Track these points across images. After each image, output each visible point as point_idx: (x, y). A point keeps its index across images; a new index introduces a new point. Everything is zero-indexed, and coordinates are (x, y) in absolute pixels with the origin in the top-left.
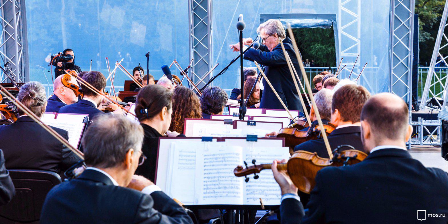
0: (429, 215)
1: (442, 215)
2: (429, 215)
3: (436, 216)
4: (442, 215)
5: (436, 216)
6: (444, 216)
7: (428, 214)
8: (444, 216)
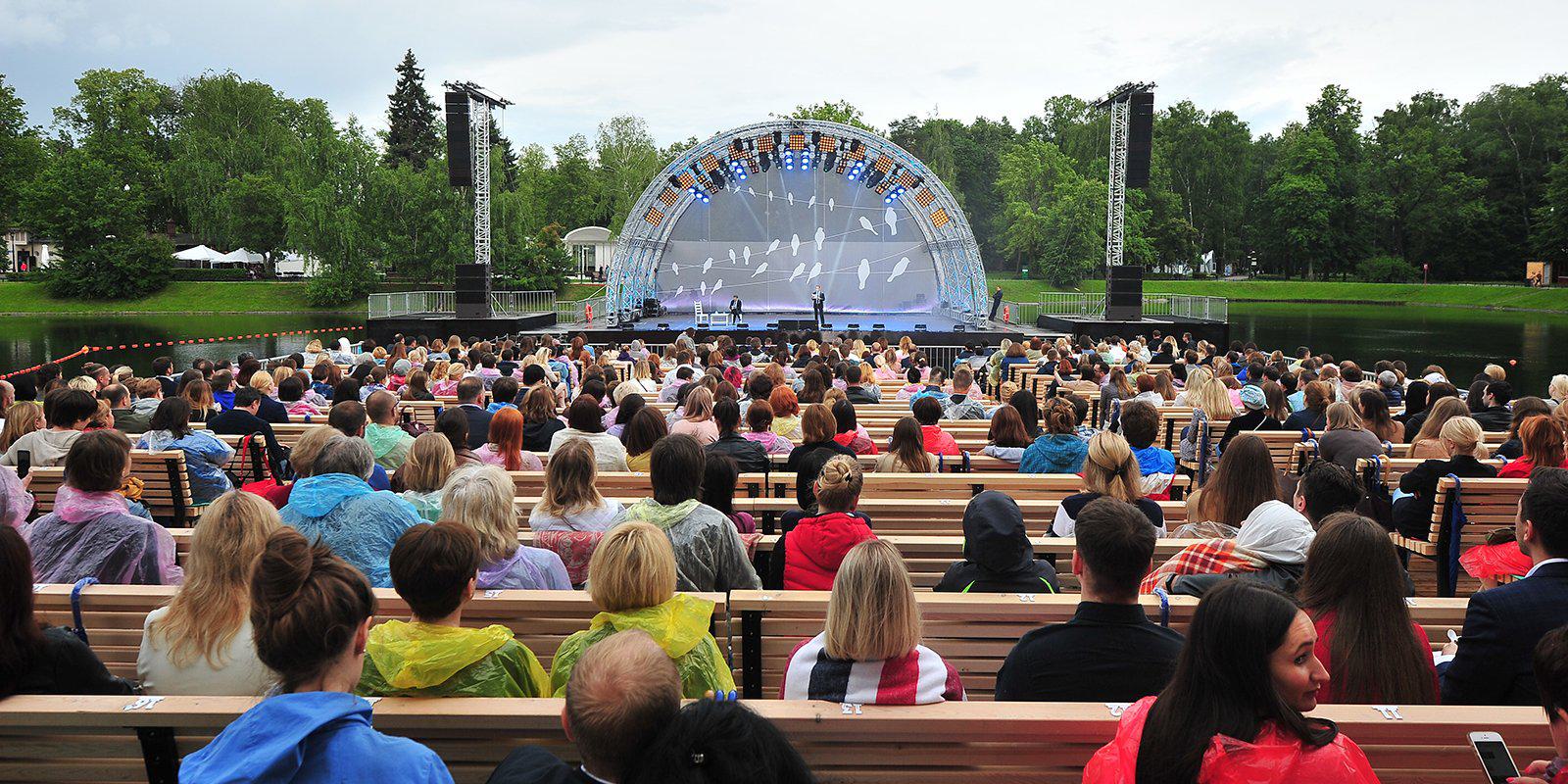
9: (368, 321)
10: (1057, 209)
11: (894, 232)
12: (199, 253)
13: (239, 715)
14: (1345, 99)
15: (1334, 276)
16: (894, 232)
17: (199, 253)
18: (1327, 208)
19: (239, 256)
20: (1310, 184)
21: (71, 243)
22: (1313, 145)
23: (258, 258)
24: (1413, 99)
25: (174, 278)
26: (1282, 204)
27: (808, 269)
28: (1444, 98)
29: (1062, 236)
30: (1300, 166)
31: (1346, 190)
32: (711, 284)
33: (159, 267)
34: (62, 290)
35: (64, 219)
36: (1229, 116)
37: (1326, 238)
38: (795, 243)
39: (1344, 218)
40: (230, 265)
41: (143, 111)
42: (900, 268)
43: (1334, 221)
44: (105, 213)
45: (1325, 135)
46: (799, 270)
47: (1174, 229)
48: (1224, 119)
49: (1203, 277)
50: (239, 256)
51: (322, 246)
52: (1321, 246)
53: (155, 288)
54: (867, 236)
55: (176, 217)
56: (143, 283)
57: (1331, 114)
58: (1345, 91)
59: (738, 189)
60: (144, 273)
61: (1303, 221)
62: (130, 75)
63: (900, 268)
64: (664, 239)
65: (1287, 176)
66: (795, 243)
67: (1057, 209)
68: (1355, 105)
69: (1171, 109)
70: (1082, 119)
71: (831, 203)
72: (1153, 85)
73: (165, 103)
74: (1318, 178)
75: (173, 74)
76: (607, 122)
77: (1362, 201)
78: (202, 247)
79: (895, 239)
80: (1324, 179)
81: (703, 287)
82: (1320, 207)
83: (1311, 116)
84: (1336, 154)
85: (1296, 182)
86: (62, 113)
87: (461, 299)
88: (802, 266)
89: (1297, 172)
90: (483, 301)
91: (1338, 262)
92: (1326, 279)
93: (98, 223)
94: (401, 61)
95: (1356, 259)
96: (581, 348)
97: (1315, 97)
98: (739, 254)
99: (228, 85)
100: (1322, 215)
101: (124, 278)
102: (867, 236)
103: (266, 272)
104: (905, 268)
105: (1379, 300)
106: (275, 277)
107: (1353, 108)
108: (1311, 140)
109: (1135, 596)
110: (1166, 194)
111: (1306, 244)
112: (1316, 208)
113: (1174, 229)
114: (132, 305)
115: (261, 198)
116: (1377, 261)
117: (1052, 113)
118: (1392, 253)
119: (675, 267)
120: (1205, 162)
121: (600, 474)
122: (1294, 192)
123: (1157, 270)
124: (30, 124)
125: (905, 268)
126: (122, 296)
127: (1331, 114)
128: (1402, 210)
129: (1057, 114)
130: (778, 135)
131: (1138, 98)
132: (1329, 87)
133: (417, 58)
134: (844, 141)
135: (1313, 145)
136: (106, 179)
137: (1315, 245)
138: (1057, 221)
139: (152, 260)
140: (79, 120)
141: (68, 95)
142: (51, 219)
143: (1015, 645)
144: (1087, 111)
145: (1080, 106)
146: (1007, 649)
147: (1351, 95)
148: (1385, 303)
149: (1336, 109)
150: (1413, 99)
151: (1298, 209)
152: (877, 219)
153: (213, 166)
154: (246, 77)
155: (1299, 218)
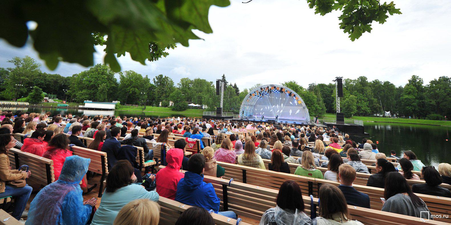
0: (432, 216)
1: (445, 216)
2: (432, 216)
3: (439, 217)
4: (445, 216)
5: (439, 217)
6: (447, 217)
7: (431, 215)
8: (447, 217)
9: (203, 116)
10: (345, 101)
11: (296, 105)
12: (192, 105)
13: (13, 147)
14: (418, 78)
15: (422, 118)
16: (296, 105)
17: (192, 105)
18: (416, 102)
19: (197, 105)
20: (410, 97)
21: (175, 102)
22: (410, 88)
23: (199, 106)
24: (439, 78)
25: (188, 108)
26: (404, 101)
27: (280, 111)
28: (448, 77)
29: (346, 107)
30: (407, 93)
31: (421, 98)
32: (262, 113)
33: (185, 107)
34: (173, 110)
35: (174, 99)
36: (388, 82)
37: (417, 109)
38: (278, 106)
39: (422, 105)
40: (196, 107)
41: (189, 84)
42: (298, 111)
43: (419, 105)
44: (179, 98)
45: (413, 86)
46: (278, 111)
47: (375, 106)
48: (387, 84)
49: (385, 117)
50: (197, 105)
51: (208, 104)
52: (416, 111)
53: (185, 110)
54: (291, 105)
55: (189, 99)
56: (183, 109)
57: (415, 83)
58: (418, 77)
59: (267, 96)
60: (183, 107)
61: (409, 105)
62: (187, 78)
63: (298, 111)
64: (254, 105)
65: (404, 95)
66: (278, 106)
67: (345, 101)
68: (421, 79)
69: (373, 81)
70: (352, 83)
71: (277, 98)
72: (342, 77)
73: (191, 82)
74: (412, 95)
75: (192, 79)
76: (256, 85)
77: (427, 101)
78: (193, 104)
79: (296, 106)
80: (414, 96)
81: (261, 113)
82: (414, 102)
83: (410, 82)
84: (417, 90)
85: (406, 96)
86: (178, 84)
87: (217, 113)
88: (279, 110)
89: (407, 94)
90: (220, 113)
91: (421, 115)
92: (419, 119)
93: (178, 100)
94: (223, 76)
95: (426, 114)
96: (211, 121)
97: (410, 78)
98: (267, 107)
99: (199, 79)
100: (415, 104)
101: (181, 108)
102: (291, 105)
103: (201, 108)
104: (296, 113)
105: (433, 124)
106: (202, 109)
107: (421, 80)
108: (409, 87)
109: (351, 184)
110: (373, 99)
111: (411, 110)
112: (413, 102)
113: (375, 106)
114: (181, 112)
115: (200, 97)
116: (432, 115)
117: (345, 82)
118: (436, 113)
119: (256, 109)
120: (382, 92)
121: (139, 135)
122: (406, 99)
123: (375, 115)
124: (174, 86)
125: (296, 113)
126: (180, 111)
127: (415, 83)
128: (438, 103)
129: (346, 82)
130: (268, 87)
131: (339, 80)
132: (413, 76)
133: (225, 75)
134: (264, 88)
135: (410, 88)
136: (180, 93)
137: (414, 111)
138: (345, 104)
139: (185, 105)
140: (180, 85)
141: (179, 81)
142: (173, 99)
143: (283, 183)
144: (353, 82)
145: (351, 81)
146: (281, 183)
147: (419, 77)
148: (434, 125)
149: (416, 80)
150: (439, 78)
151: (408, 102)
152: (293, 102)
153: (195, 92)
154: (201, 78)
155: (408, 104)
